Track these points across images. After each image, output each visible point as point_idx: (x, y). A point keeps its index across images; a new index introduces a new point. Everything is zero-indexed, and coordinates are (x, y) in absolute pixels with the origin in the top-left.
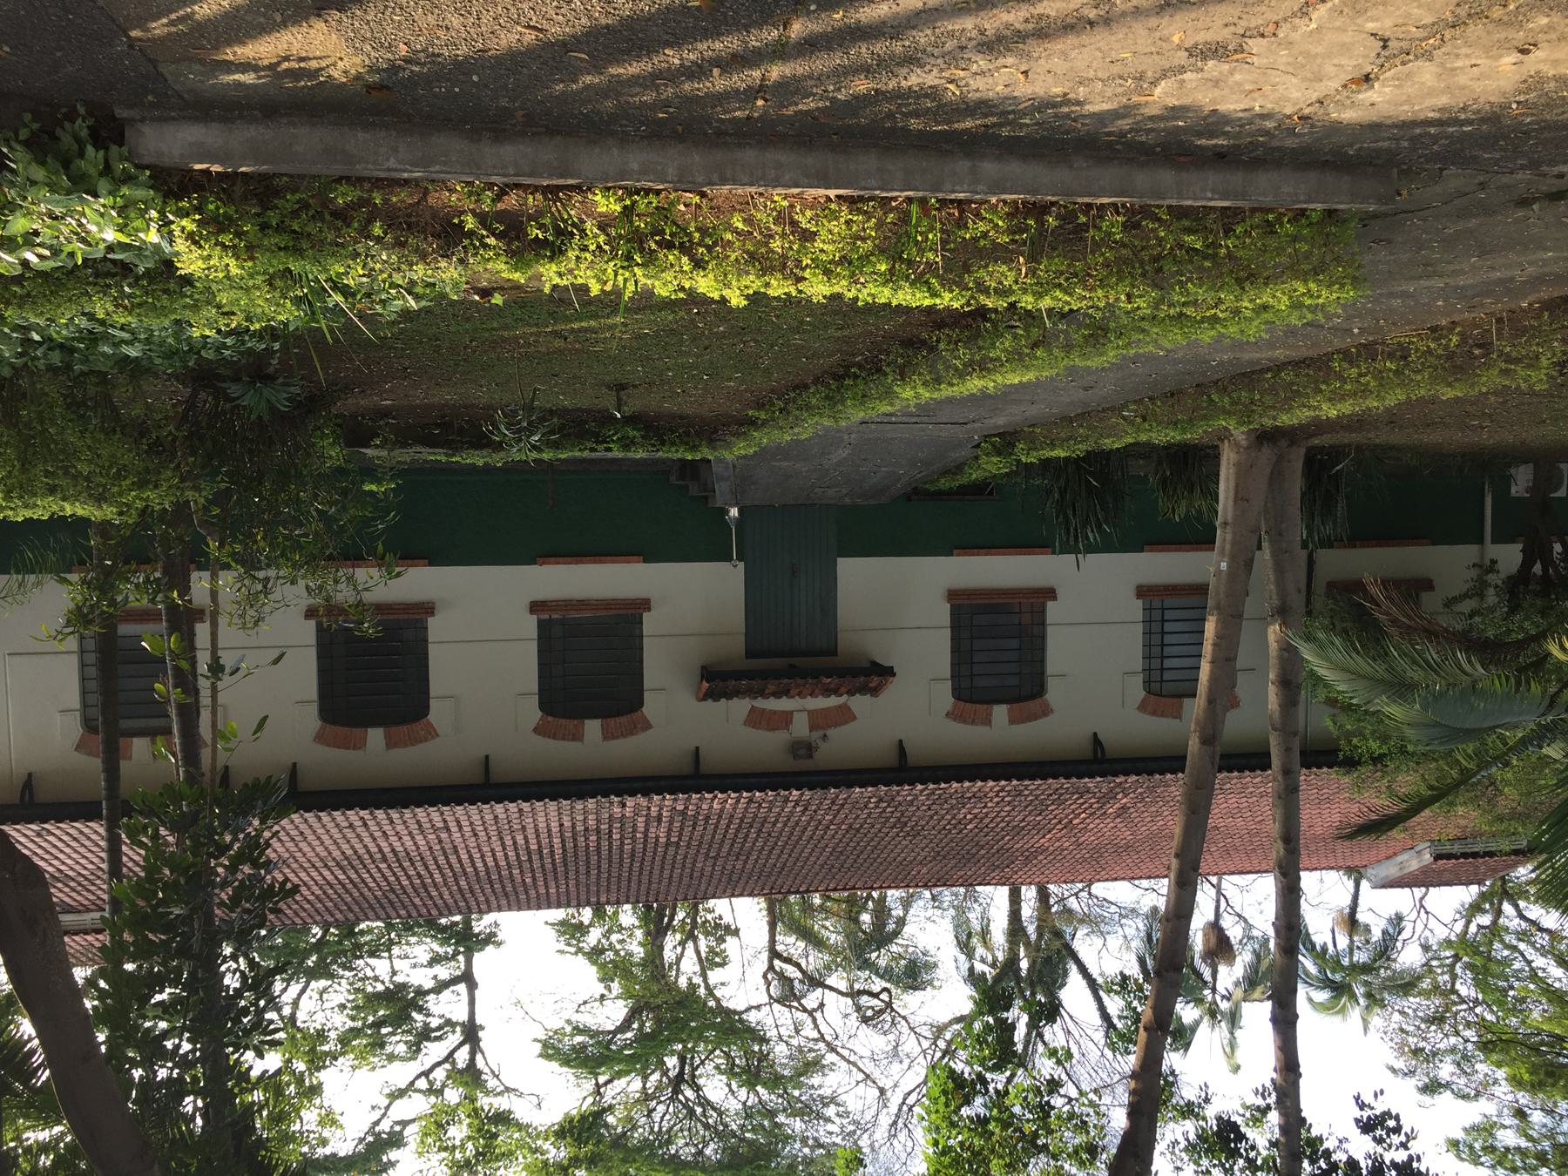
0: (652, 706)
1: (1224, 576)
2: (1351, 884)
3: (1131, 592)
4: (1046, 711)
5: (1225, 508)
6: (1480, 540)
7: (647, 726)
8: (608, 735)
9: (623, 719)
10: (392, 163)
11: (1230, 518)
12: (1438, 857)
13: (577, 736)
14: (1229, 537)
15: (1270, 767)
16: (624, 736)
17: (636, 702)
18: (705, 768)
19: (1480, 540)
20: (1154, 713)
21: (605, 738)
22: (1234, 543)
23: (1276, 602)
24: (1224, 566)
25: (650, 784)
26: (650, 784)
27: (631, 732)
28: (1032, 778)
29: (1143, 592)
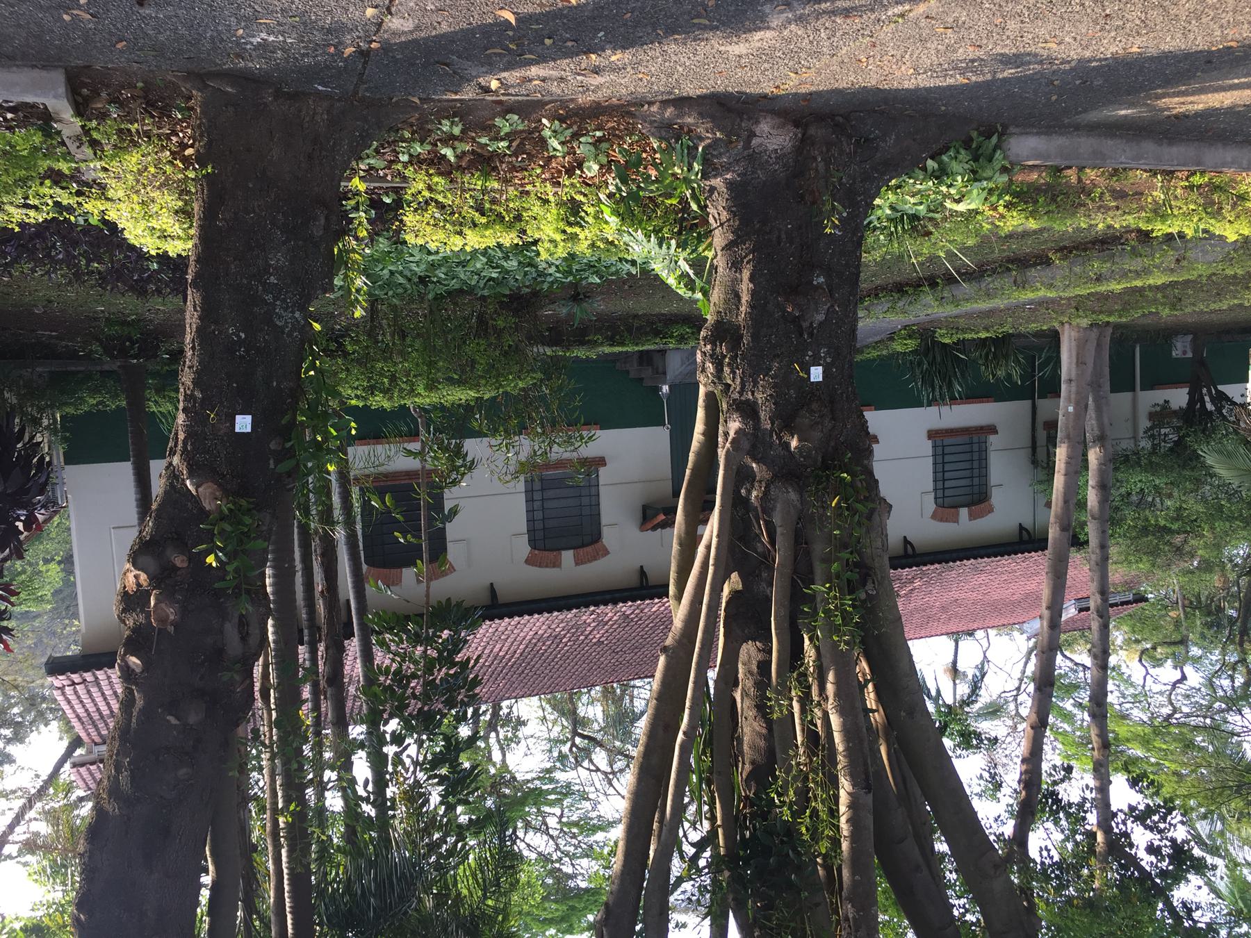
0: (609, 537)
1: (1072, 417)
2: (953, 644)
3: (925, 435)
4: (991, 510)
5: (1069, 370)
6: (1133, 389)
7: (606, 552)
8: (578, 562)
9: (589, 549)
10: (1123, 159)
11: (1073, 376)
12: (1081, 610)
13: (556, 564)
14: (1074, 389)
15: (1044, 548)
16: (590, 561)
17: (596, 537)
18: (502, 599)
19: (1133, 389)
20: (941, 520)
21: (577, 564)
22: (1078, 393)
23: (1097, 432)
24: (1071, 409)
25: (598, 598)
26: (598, 598)
27: (595, 558)
28: (932, 564)
29: (932, 434)
